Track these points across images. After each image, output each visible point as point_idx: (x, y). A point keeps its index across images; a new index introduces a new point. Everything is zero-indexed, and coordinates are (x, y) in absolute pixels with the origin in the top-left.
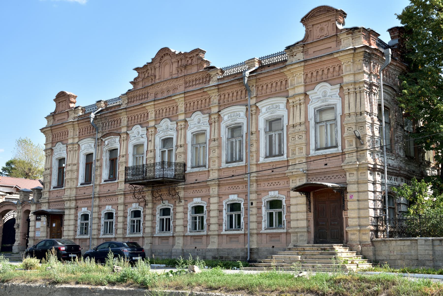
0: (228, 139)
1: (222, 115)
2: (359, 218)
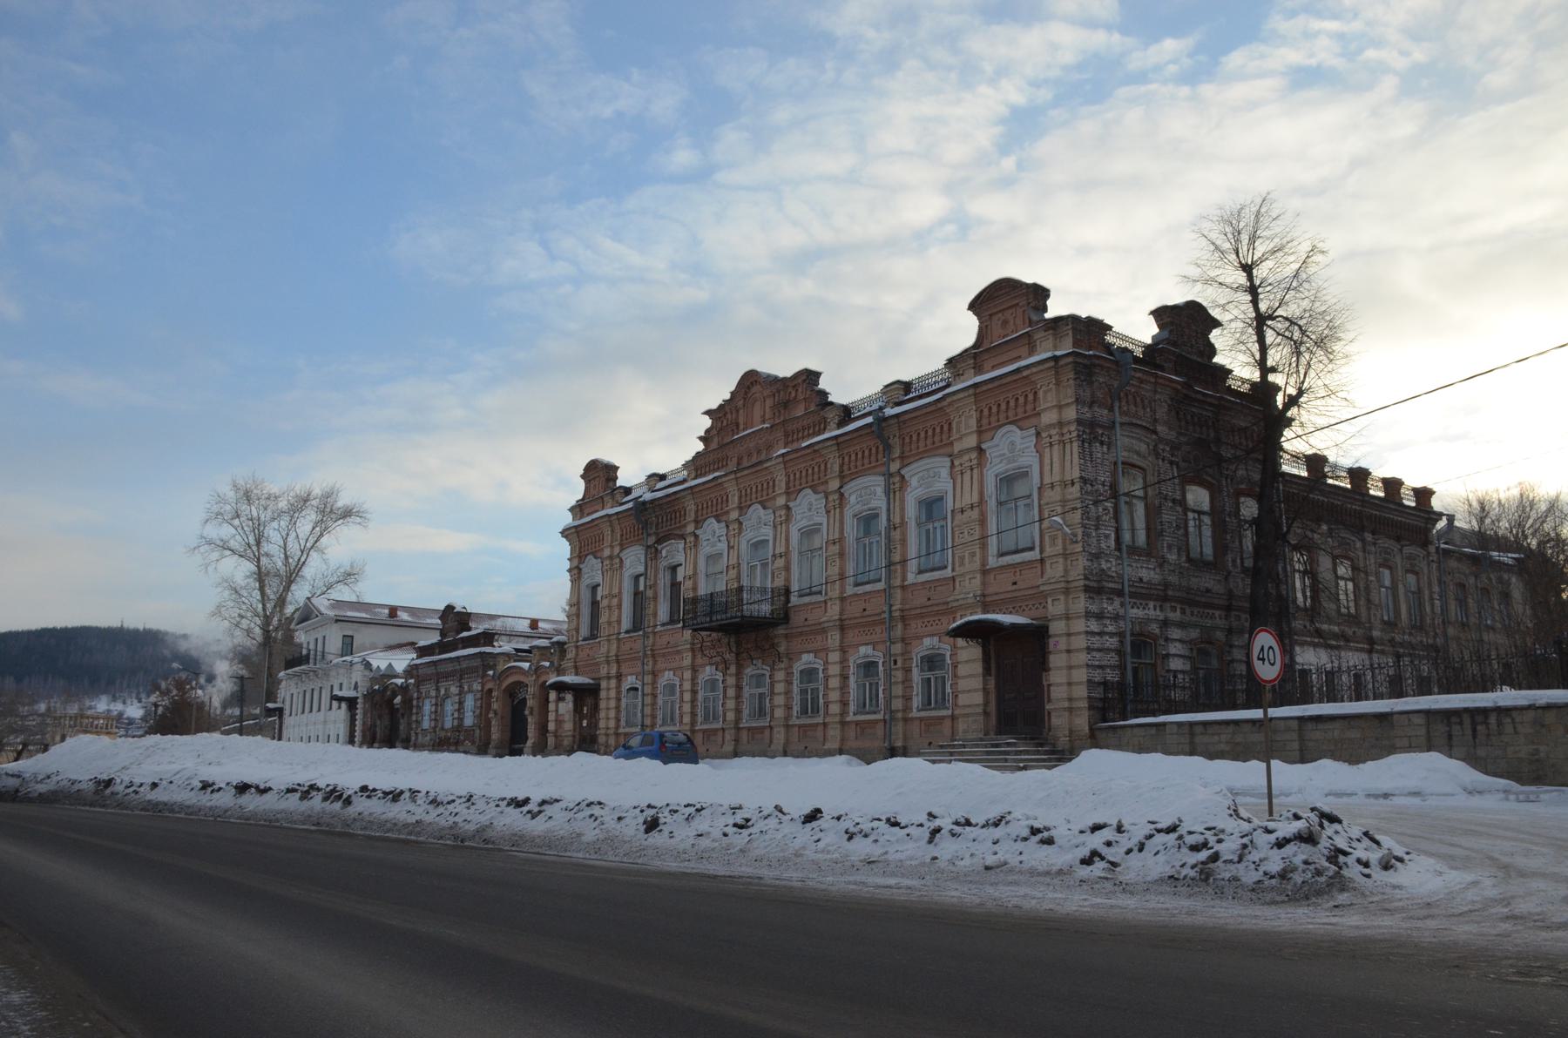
0: (858, 539)
2: (1070, 684)
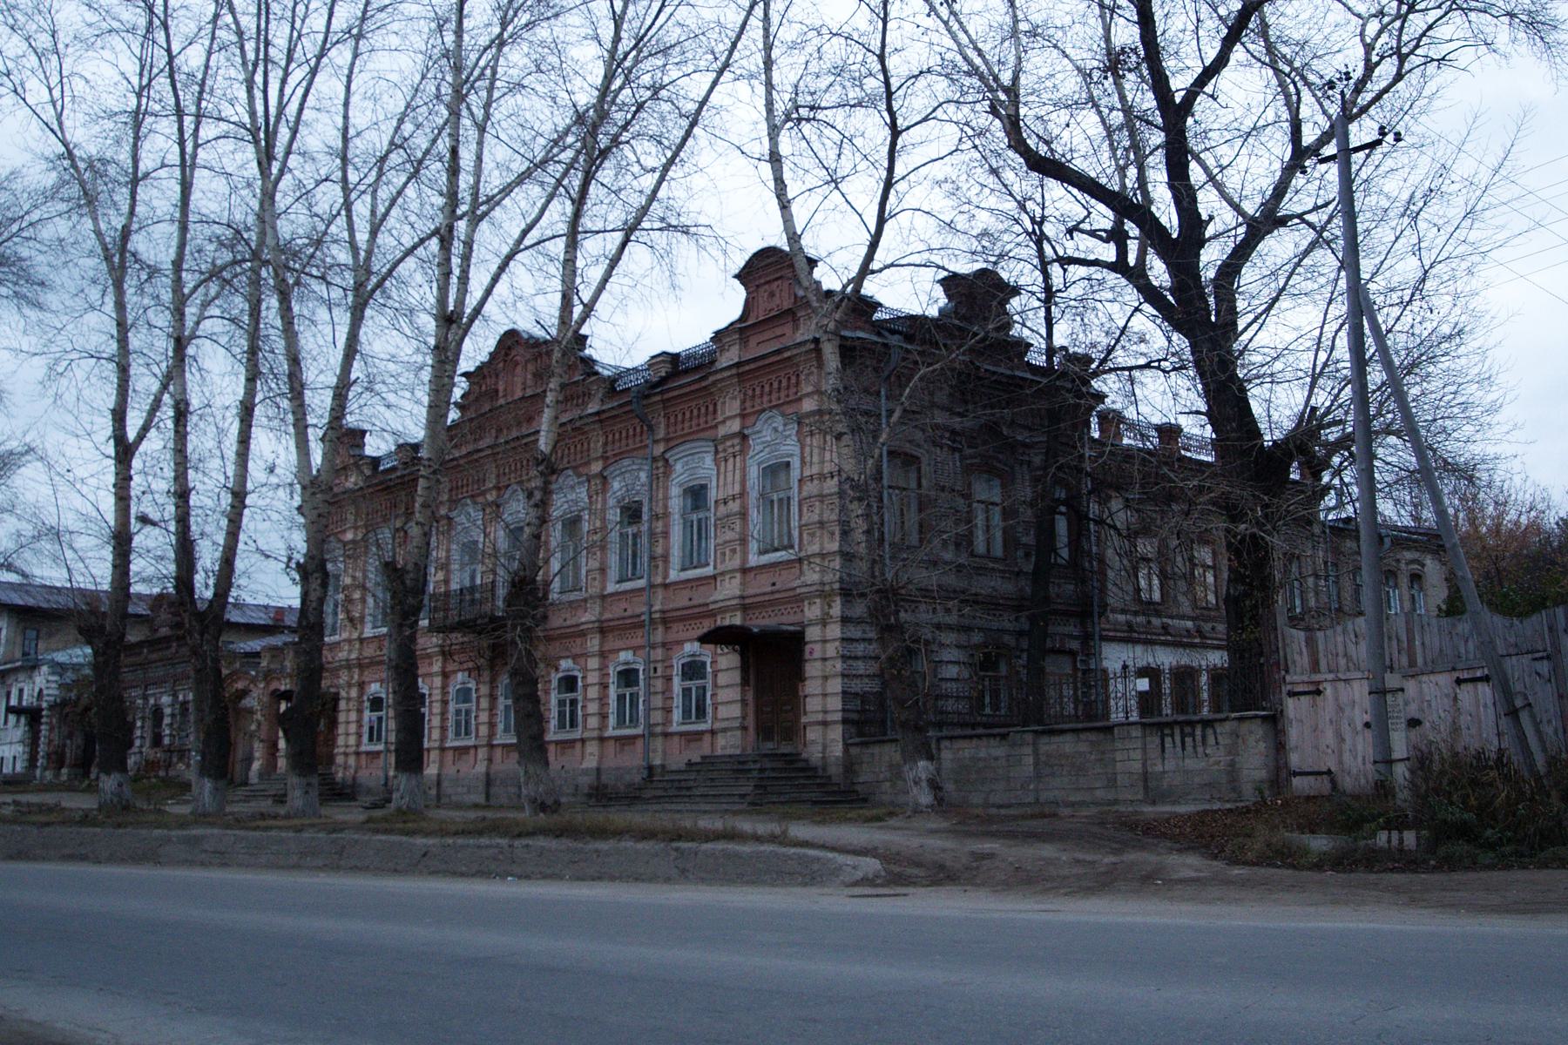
1: (671, 461)
